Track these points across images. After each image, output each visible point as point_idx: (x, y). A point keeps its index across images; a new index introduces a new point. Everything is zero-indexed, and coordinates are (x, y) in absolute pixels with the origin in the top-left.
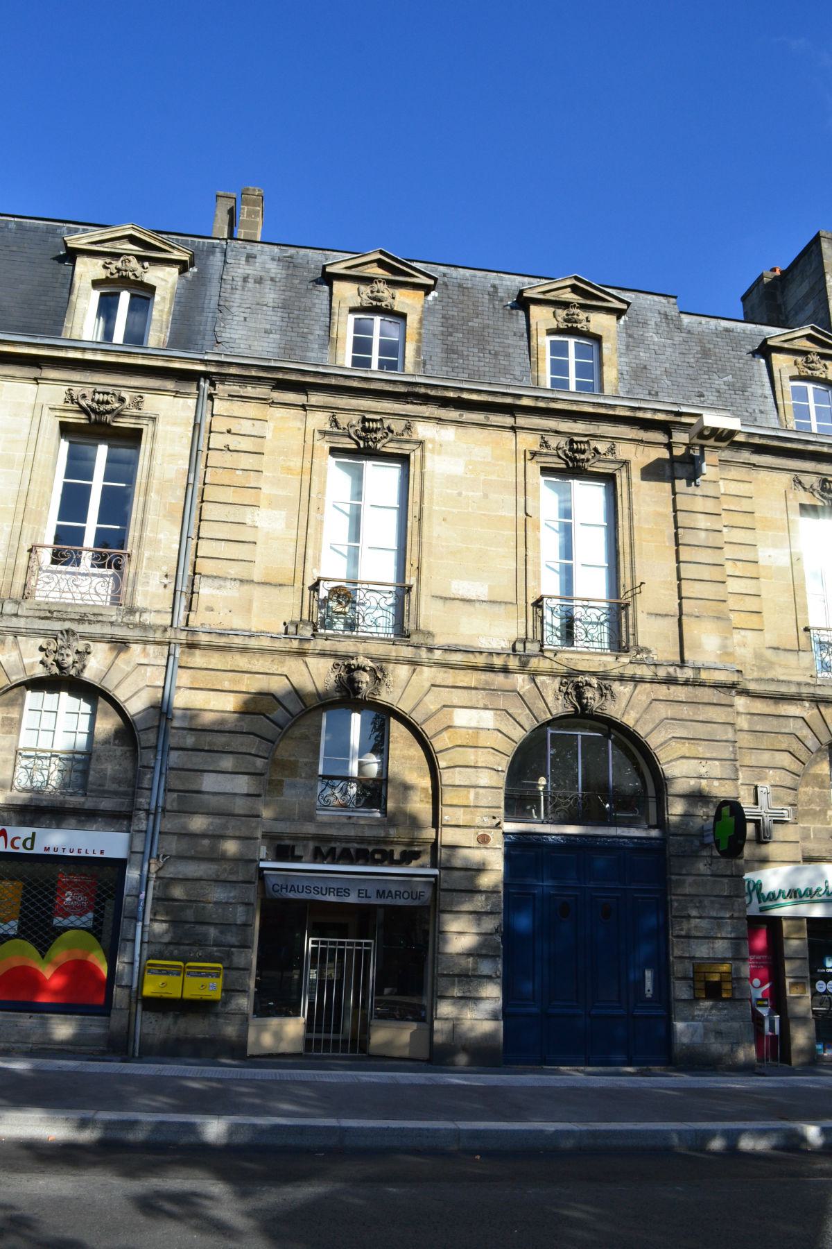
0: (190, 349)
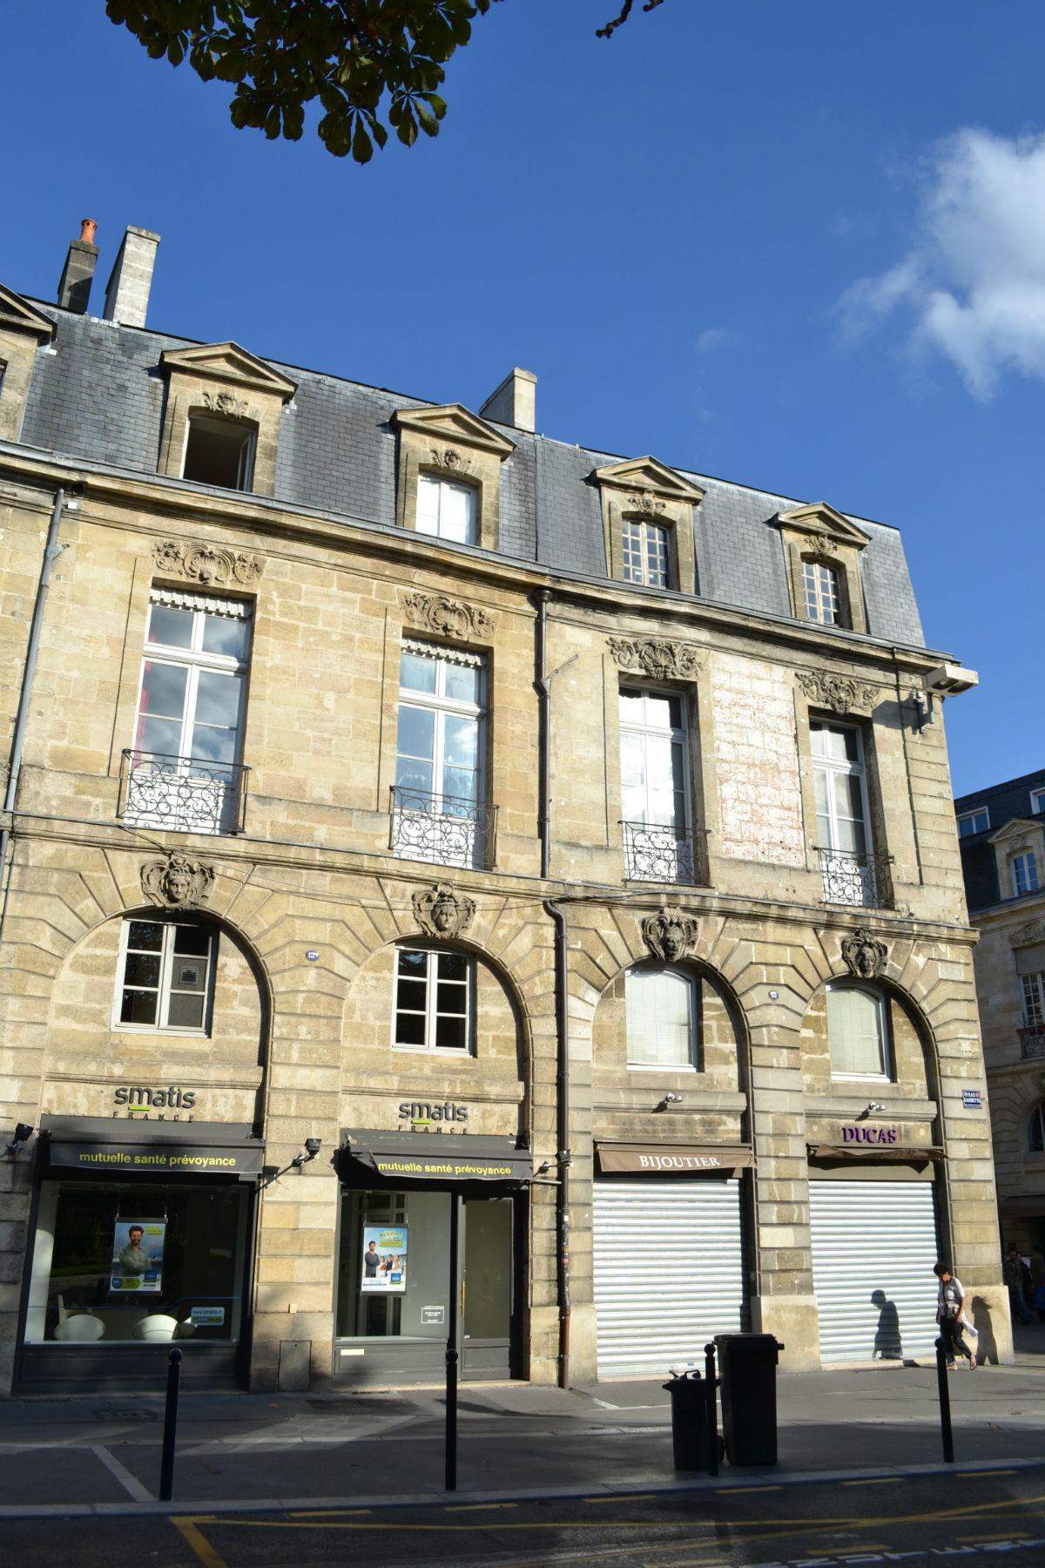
0: (316, 503)
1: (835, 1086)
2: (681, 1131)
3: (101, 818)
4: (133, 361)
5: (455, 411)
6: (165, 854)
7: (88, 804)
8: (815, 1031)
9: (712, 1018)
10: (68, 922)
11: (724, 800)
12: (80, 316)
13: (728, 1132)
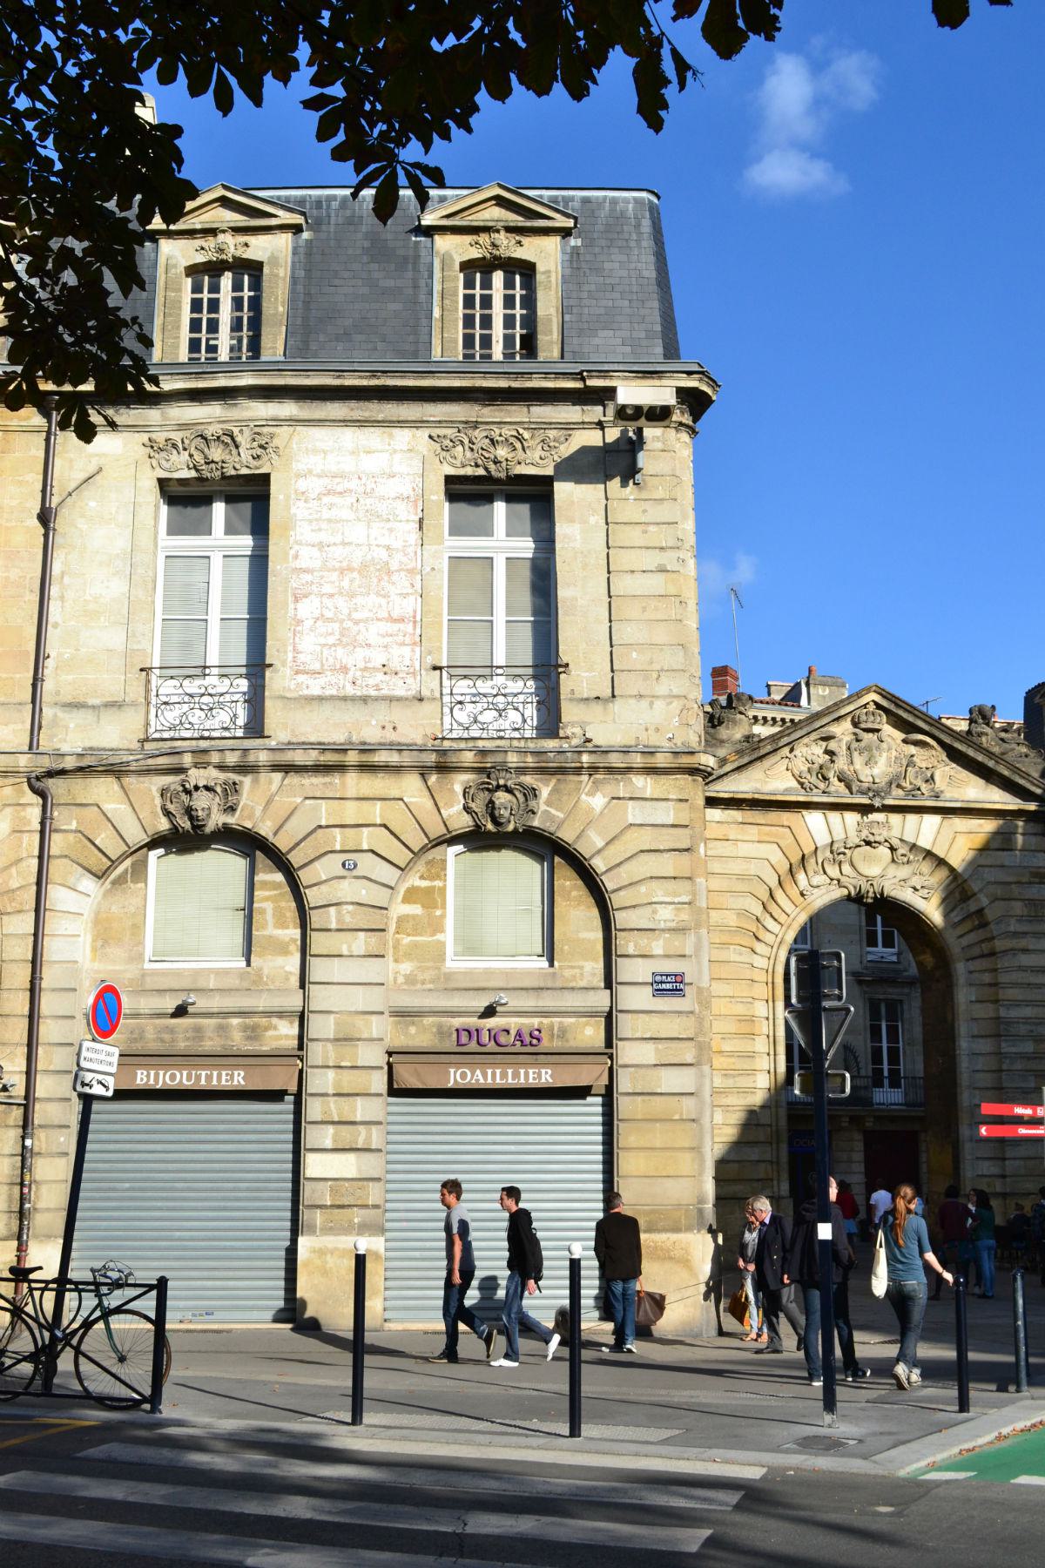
1: (449, 976)
2: (211, 1039)
8: (423, 906)
9: (267, 899)
11: (299, 622)
13: (279, 1038)
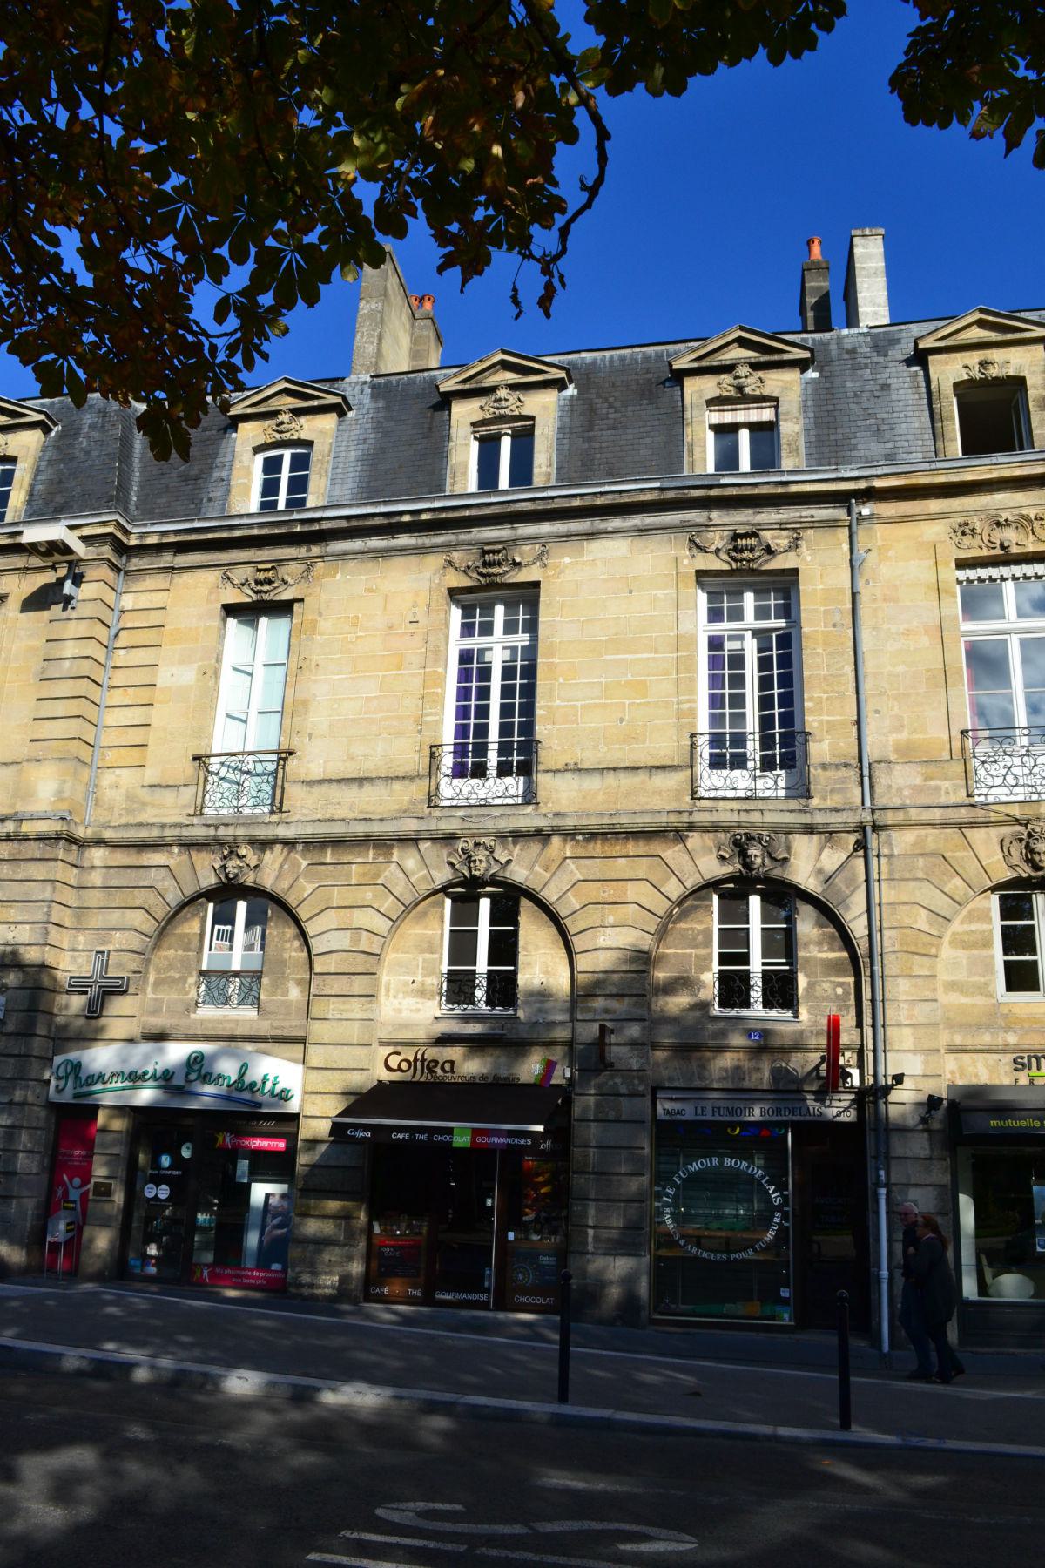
3: (953, 800)
4: (889, 358)
5: (978, 316)
6: (1021, 825)
7: (938, 789)
10: (941, 903)
12: (831, 333)
